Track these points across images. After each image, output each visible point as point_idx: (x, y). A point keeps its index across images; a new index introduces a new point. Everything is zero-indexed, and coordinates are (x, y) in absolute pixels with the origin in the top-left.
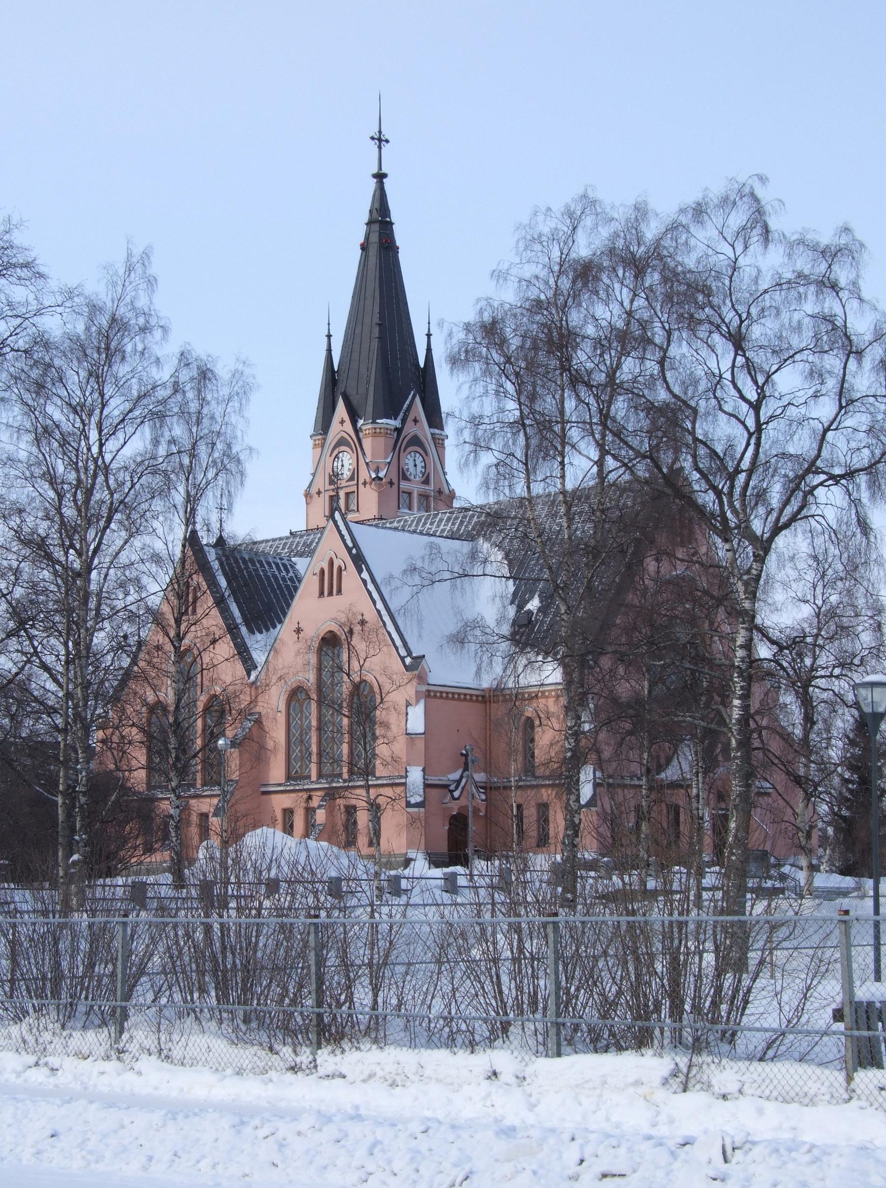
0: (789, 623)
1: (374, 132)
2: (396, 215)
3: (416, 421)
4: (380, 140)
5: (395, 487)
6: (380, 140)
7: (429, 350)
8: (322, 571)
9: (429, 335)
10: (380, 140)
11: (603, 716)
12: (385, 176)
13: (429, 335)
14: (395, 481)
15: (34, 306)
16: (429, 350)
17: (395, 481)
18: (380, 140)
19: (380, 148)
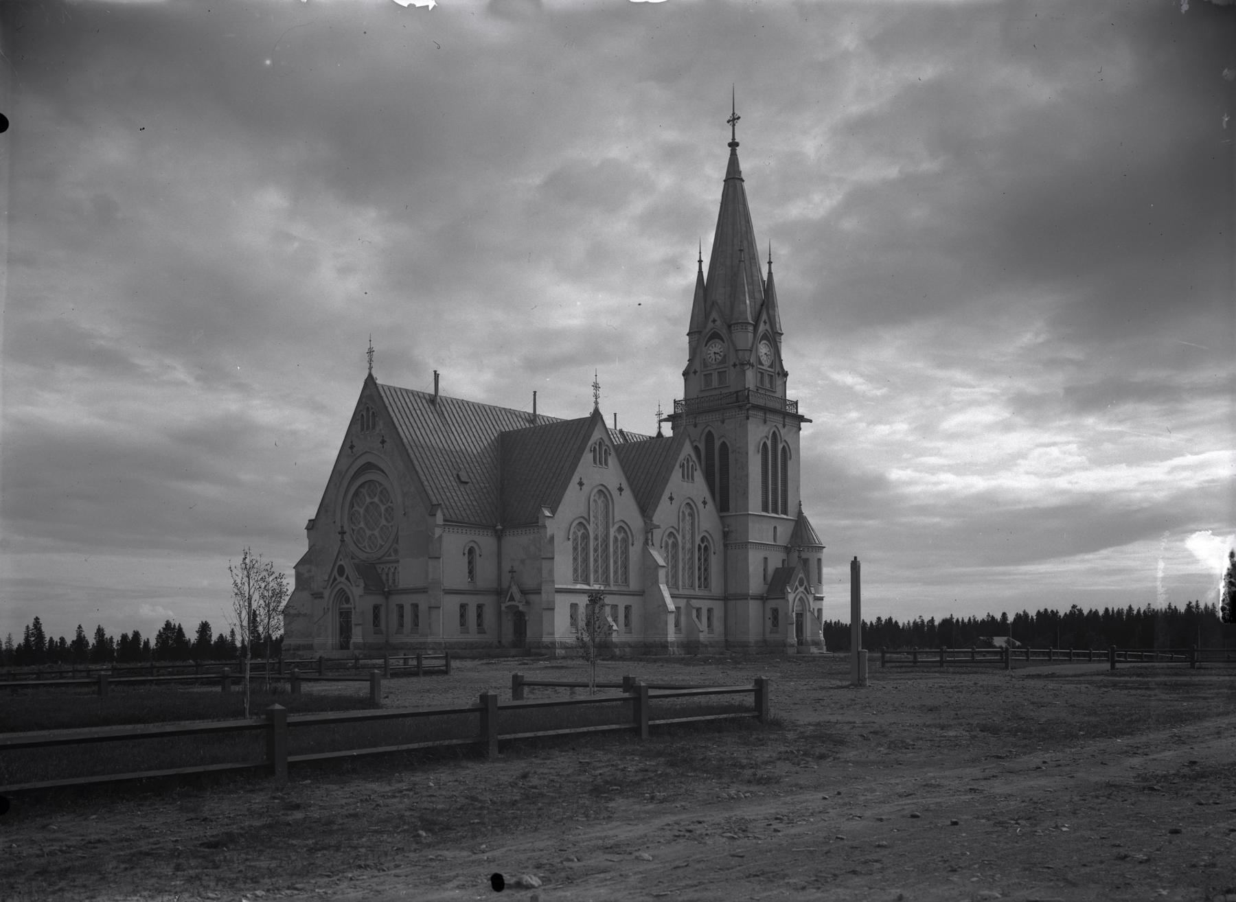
7: (770, 273)
16: (770, 273)
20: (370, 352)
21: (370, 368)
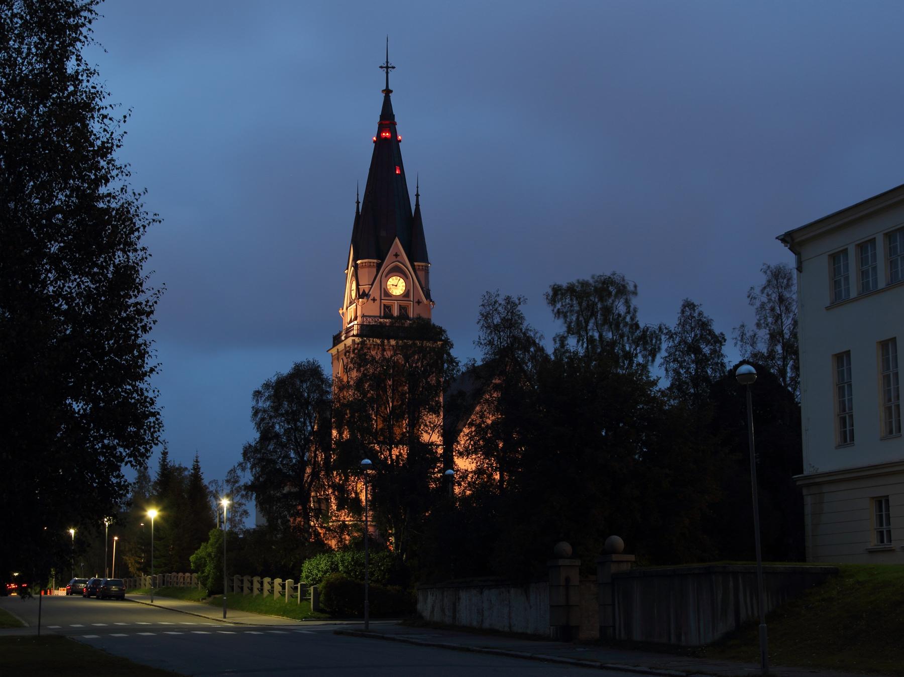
1: (383, 62)
3: (396, 255)
4: (387, 68)
5: (378, 302)
6: (387, 67)
7: (417, 205)
9: (417, 195)
13: (417, 195)
16: (417, 205)
17: (378, 298)
18: (387, 67)
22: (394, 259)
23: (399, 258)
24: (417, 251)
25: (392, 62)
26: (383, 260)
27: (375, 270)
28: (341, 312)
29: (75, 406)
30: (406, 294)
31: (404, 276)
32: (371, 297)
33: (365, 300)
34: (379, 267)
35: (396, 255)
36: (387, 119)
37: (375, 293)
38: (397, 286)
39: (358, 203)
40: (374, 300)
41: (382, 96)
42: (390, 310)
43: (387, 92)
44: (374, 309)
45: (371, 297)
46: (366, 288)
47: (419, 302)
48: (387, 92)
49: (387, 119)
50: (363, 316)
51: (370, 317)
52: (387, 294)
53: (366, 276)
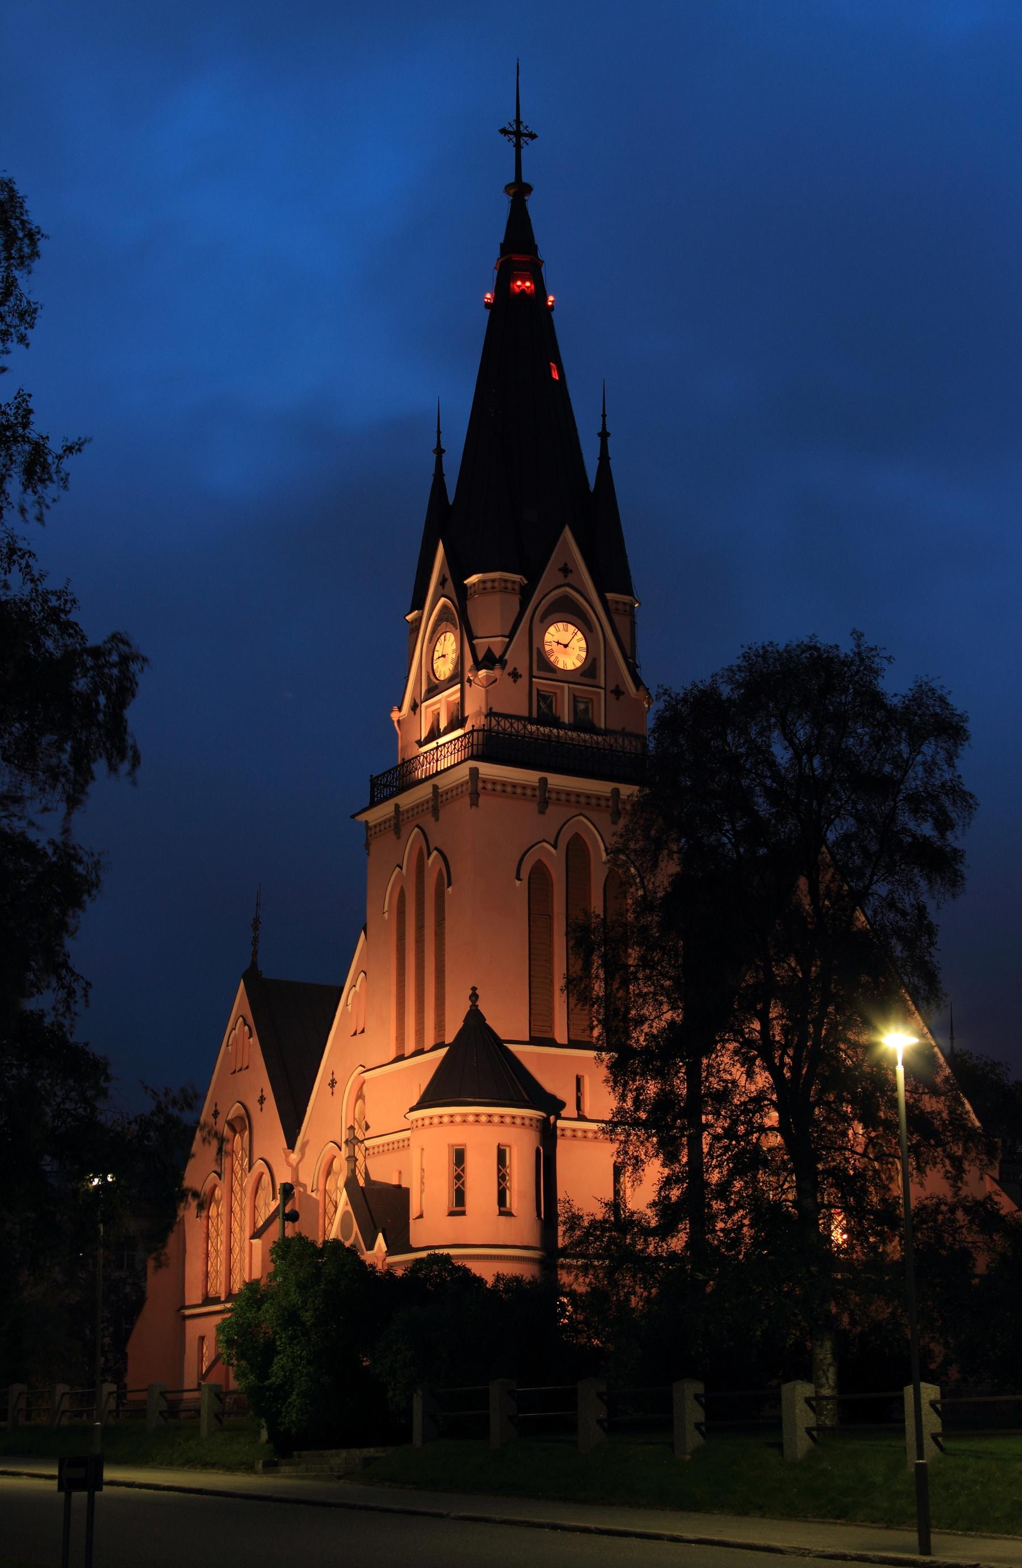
0: (654, 722)
1: (507, 119)
2: (611, 453)
3: (566, 570)
4: (518, 134)
5: (524, 681)
6: (518, 134)
7: (604, 458)
8: (421, 849)
9: (604, 435)
10: (518, 134)
11: (770, 649)
12: (527, 189)
13: (604, 435)
14: (523, 670)
15: (666, 698)
16: (604, 458)
17: (523, 670)
18: (518, 134)
19: (518, 147)
20: (256, 923)
21: (255, 953)
22: (560, 578)
23: (570, 579)
24: (611, 571)
25: (529, 122)
26: (534, 579)
27: (515, 601)
28: (395, 716)
29: (849, 1110)
30: (588, 670)
31: (585, 626)
32: (509, 668)
33: (497, 673)
34: (525, 594)
35: (566, 570)
36: (519, 248)
37: (518, 658)
38: (567, 647)
39: (439, 451)
40: (515, 675)
41: (505, 203)
42: (550, 707)
43: (519, 191)
44: (516, 700)
45: (509, 668)
46: (496, 644)
47: (618, 692)
48: (519, 191)
49: (519, 248)
50: (490, 714)
51: (506, 716)
52: (544, 664)
53: (491, 618)
